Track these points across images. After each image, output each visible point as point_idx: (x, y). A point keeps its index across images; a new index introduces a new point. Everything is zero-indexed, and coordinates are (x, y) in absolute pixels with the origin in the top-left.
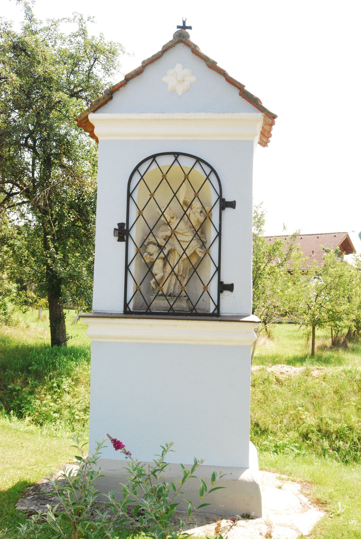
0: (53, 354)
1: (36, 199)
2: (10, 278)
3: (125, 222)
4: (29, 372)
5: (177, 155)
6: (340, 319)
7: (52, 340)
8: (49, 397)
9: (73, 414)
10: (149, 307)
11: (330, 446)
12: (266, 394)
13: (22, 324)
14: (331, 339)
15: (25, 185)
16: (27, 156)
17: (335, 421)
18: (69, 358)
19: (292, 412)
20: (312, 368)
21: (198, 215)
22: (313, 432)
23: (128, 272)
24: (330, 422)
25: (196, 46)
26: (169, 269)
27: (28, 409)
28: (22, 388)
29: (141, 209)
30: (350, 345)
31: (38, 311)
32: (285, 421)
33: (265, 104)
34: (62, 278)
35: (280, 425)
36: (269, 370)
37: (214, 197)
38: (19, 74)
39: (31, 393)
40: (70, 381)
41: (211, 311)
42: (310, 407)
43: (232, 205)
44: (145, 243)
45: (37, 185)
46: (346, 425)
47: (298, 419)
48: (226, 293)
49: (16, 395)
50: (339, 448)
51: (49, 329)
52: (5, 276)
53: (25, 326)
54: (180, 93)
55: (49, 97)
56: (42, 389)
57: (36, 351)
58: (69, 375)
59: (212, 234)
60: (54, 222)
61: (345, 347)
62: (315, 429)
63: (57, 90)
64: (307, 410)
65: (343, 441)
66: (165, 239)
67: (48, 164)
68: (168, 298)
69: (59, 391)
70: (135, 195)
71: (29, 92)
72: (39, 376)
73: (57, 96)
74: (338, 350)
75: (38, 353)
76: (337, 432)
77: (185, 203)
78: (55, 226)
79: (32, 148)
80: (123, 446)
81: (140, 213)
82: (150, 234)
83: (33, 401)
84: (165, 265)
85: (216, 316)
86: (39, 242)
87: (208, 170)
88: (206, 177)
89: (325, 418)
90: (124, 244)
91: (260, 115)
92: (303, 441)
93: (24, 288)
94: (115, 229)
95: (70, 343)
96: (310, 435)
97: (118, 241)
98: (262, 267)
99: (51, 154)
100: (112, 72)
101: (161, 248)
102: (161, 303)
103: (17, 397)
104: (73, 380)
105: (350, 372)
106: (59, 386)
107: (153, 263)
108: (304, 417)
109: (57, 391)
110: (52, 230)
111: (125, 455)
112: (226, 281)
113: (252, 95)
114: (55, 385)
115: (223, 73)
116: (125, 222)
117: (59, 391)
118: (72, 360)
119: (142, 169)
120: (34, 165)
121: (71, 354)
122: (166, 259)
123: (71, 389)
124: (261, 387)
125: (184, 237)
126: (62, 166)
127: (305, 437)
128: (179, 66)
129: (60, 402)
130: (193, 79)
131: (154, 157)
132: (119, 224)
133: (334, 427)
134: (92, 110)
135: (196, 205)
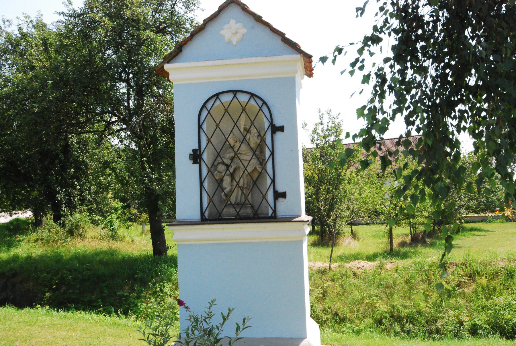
0: (155, 263)
1: (132, 127)
2: (115, 197)
3: (197, 148)
4: (135, 280)
5: (235, 92)
6: (414, 217)
7: (154, 250)
8: (153, 300)
9: (175, 314)
10: (220, 214)
11: (402, 329)
12: (344, 286)
13: (128, 239)
14: (410, 236)
15: (122, 115)
16: (122, 88)
17: (405, 307)
18: (170, 265)
19: (367, 301)
20: (385, 261)
21: (255, 138)
22: (386, 317)
23: (203, 189)
24: (401, 308)
25: (244, 5)
26: (235, 184)
27: (135, 311)
28: (130, 294)
29: (209, 137)
30: (428, 240)
31: (141, 226)
32: (361, 310)
33: (302, 48)
34: (158, 194)
35: (357, 313)
36: (347, 265)
37: (267, 124)
38: (111, 17)
39: (138, 297)
40: (171, 285)
41: (270, 215)
42: (384, 296)
43: (281, 129)
44: (216, 164)
45: (131, 113)
46: (415, 310)
47: (372, 307)
48: (281, 200)
49: (125, 300)
50: (410, 330)
51: (151, 240)
52: (110, 196)
53: (130, 240)
54: (235, 43)
55: (138, 35)
56: (147, 293)
57: (140, 260)
58: (169, 280)
59: (268, 153)
60: (149, 146)
61: (424, 243)
62: (388, 315)
63: (145, 30)
64: (380, 299)
65: (412, 324)
66: (230, 159)
67: (140, 95)
68: (235, 206)
69: (162, 295)
70: (204, 127)
71: (120, 32)
72: (144, 283)
73: (145, 34)
74: (417, 246)
75: (142, 263)
76: (407, 317)
77: (245, 129)
78: (149, 149)
79: (127, 81)
80: (184, 304)
81: (209, 141)
82: (217, 157)
83: (139, 304)
84: (232, 181)
85: (274, 218)
86: (137, 165)
87: (260, 103)
88: (259, 108)
89: (396, 305)
90: (197, 166)
91: (299, 56)
92: (377, 326)
93: (128, 206)
94: (190, 154)
95: (170, 253)
96: (383, 321)
97: (194, 163)
98: (343, 174)
99: (143, 86)
100: (192, 8)
101: (228, 166)
102: (230, 211)
103: (126, 302)
104: (173, 285)
105: (419, 263)
106: (161, 291)
107: (222, 180)
108: (377, 305)
109: (159, 295)
110: (148, 153)
111: (186, 309)
112: (280, 189)
113: (291, 41)
114: (158, 289)
115: (267, 25)
116: (197, 148)
117: (162, 295)
118: (172, 267)
119: (209, 105)
120: (129, 94)
121: (171, 262)
122: (232, 175)
123: (172, 293)
124: (340, 281)
125: (246, 156)
126: (153, 95)
127: (379, 322)
128: (232, 22)
129: (163, 304)
130: (244, 31)
131: (217, 96)
132: (193, 150)
133: (404, 312)
134: (167, 61)
135: (253, 130)
